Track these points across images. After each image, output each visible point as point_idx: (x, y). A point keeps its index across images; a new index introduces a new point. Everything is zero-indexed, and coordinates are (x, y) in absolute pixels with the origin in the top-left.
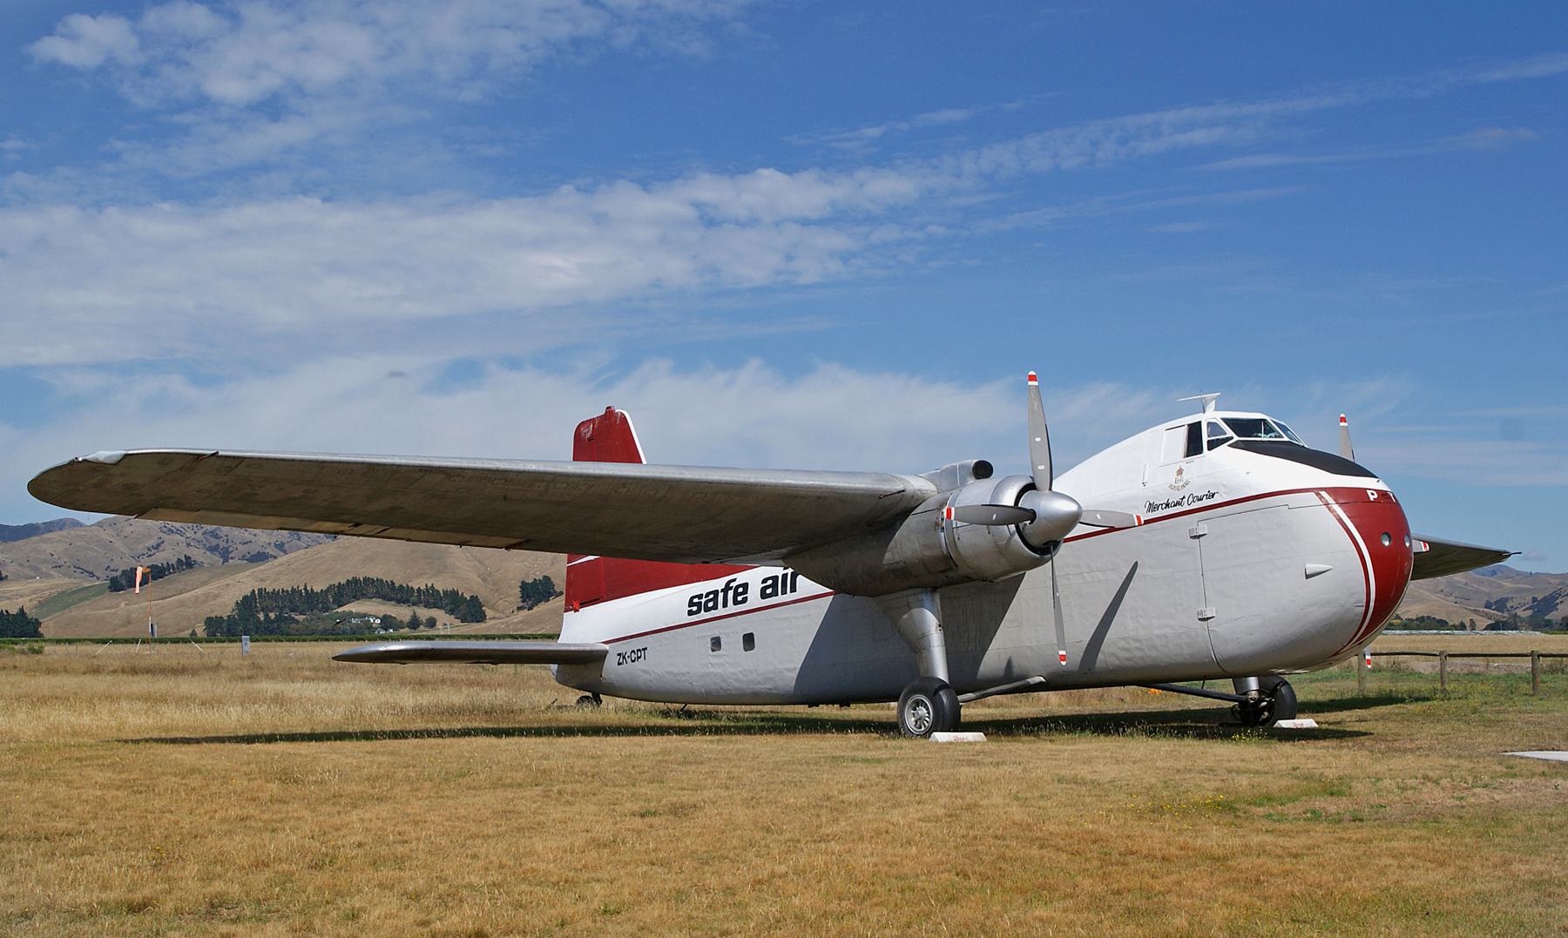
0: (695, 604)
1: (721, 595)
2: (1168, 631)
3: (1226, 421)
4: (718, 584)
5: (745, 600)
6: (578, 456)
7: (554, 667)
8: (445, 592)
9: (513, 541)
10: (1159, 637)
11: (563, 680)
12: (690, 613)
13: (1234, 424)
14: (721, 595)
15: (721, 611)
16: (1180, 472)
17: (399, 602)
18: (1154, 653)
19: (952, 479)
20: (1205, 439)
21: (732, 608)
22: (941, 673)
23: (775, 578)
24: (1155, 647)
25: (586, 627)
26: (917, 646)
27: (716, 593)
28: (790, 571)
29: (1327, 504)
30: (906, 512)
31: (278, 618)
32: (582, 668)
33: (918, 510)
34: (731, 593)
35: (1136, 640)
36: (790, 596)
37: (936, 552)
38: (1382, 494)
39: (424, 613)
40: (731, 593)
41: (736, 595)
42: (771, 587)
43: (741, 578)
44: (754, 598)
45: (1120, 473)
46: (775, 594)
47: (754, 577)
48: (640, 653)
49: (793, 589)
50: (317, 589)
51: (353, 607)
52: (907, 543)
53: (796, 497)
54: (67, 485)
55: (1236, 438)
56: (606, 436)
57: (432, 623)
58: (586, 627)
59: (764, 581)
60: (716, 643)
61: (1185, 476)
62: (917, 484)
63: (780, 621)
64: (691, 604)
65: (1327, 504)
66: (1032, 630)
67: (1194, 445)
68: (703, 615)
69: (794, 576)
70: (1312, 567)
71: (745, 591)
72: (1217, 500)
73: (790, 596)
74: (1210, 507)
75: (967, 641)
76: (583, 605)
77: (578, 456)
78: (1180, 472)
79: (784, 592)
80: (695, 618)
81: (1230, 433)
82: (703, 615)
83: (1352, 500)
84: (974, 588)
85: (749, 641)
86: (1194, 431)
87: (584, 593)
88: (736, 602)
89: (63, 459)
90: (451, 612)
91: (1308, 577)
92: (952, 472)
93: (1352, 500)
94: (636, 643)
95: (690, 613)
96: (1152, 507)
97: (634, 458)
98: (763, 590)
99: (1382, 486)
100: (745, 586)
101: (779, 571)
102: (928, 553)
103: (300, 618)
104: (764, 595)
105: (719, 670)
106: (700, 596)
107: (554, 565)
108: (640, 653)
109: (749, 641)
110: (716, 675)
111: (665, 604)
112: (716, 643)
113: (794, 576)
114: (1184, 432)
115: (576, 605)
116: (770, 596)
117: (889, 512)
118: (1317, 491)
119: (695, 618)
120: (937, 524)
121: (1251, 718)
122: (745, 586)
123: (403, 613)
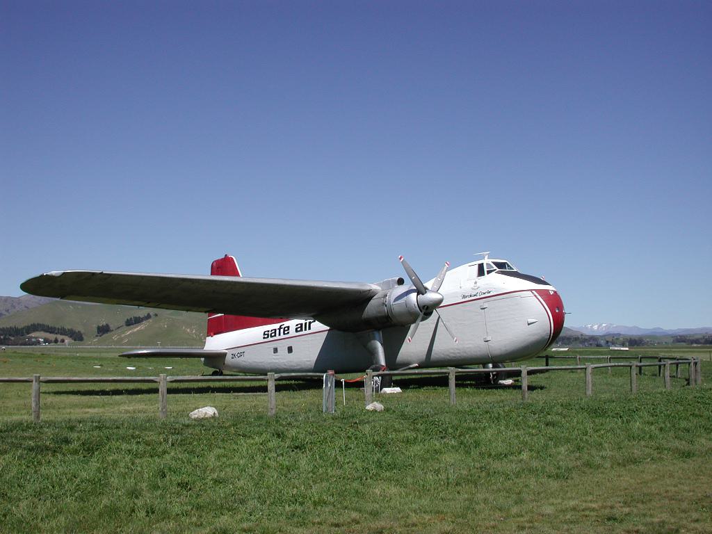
0: (266, 335)
1: (278, 331)
2: (470, 346)
3: (494, 263)
4: (276, 326)
5: (288, 333)
6: (212, 274)
7: (203, 359)
8: (69, 330)
9: (208, 309)
10: (468, 348)
11: (206, 364)
12: (264, 338)
13: (496, 264)
14: (278, 331)
15: (278, 337)
16: (476, 283)
17: (51, 333)
18: (465, 354)
19: (388, 285)
20: (486, 270)
21: (282, 336)
22: (383, 362)
23: (302, 324)
24: (465, 352)
25: (217, 343)
26: (373, 353)
27: (275, 330)
28: (308, 321)
29: (535, 296)
30: (371, 298)
31: (4, 338)
32: (215, 360)
33: (374, 298)
34: (282, 330)
35: (452, 349)
36: (308, 331)
37: (383, 314)
38: (555, 292)
39: (60, 337)
40: (282, 330)
41: (284, 331)
42: (300, 328)
43: (286, 324)
44: (292, 332)
45: (454, 282)
46: (301, 330)
47: (293, 323)
48: (241, 354)
49: (310, 329)
50: (20, 327)
51: (33, 335)
52: (372, 308)
53: (328, 292)
54: (36, 286)
55: (498, 270)
56: (224, 266)
57: (63, 341)
58: (217, 343)
59: (297, 325)
60: (276, 350)
61: (478, 284)
62: (374, 287)
63: (304, 341)
64: (264, 334)
65: (535, 296)
66: (414, 346)
67: (481, 271)
68: (270, 339)
69: (310, 323)
70: (530, 321)
71: (288, 329)
72: (491, 294)
73: (308, 331)
74: (488, 297)
75: (392, 349)
76: (215, 334)
77: (212, 274)
78: (476, 283)
79: (305, 329)
80: (266, 340)
81: (495, 267)
82: (270, 339)
83: (543, 294)
84: (394, 326)
85: (290, 350)
86: (481, 267)
87: (216, 328)
88: (284, 334)
89: (37, 274)
90: (71, 337)
91: (529, 324)
92: (388, 282)
93: (543, 294)
94: (240, 349)
95: (264, 338)
96: (464, 297)
97: (237, 274)
98: (296, 329)
99: (554, 289)
100: (288, 327)
101: (303, 322)
102: (379, 315)
103: (13, 338)
104: (297, 331)
105: (277, 361)
106: (268, 331)
107: (202, 318)
108: (241, 354)
109: (290, 350)
110: (276, 363)
111: (253, 334)
112: (276, 350)
113: (310, 323)
114: (477, 266)
115: (212, 334)
116: (300, 331)
117: (363, 298)
118: (531, 290)
119: (266, 340)
120: (384, 304)
121: (485, 382)
122: (288, 327)
123: (52, 337)
